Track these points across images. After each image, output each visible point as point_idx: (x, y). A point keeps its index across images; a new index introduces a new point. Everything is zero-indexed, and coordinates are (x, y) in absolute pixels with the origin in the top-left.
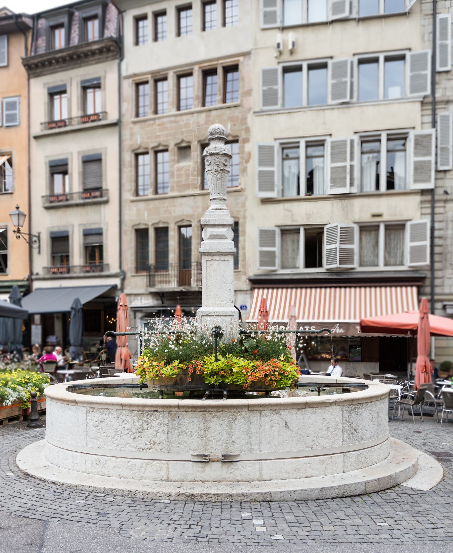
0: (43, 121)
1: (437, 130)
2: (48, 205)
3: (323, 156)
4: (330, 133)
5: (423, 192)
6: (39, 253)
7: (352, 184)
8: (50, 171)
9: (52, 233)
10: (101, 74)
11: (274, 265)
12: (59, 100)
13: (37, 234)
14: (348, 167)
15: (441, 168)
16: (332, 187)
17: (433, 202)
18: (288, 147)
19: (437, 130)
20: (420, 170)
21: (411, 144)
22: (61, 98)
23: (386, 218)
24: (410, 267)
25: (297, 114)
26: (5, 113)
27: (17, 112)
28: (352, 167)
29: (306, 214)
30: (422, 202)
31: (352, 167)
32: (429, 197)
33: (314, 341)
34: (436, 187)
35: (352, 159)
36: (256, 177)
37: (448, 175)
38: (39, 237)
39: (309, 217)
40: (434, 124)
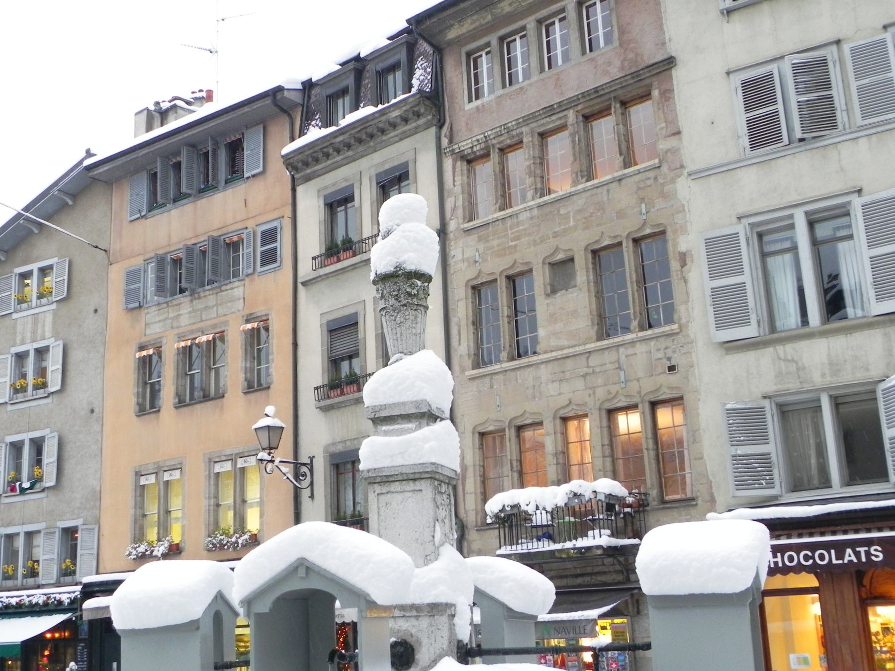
3: (850, 237)
4: (858, 185)
6: (312, 496)
8: (331, 348)
9: (333, 456)
10: (408, 157)
11: (771, 484)
12: (343, 213)
13: (308, 461)
16: (879, 298)
18: (768, 236)
27: (277, 244)
33: (70, 635)
36: (709, 301)
39: (839, 370)
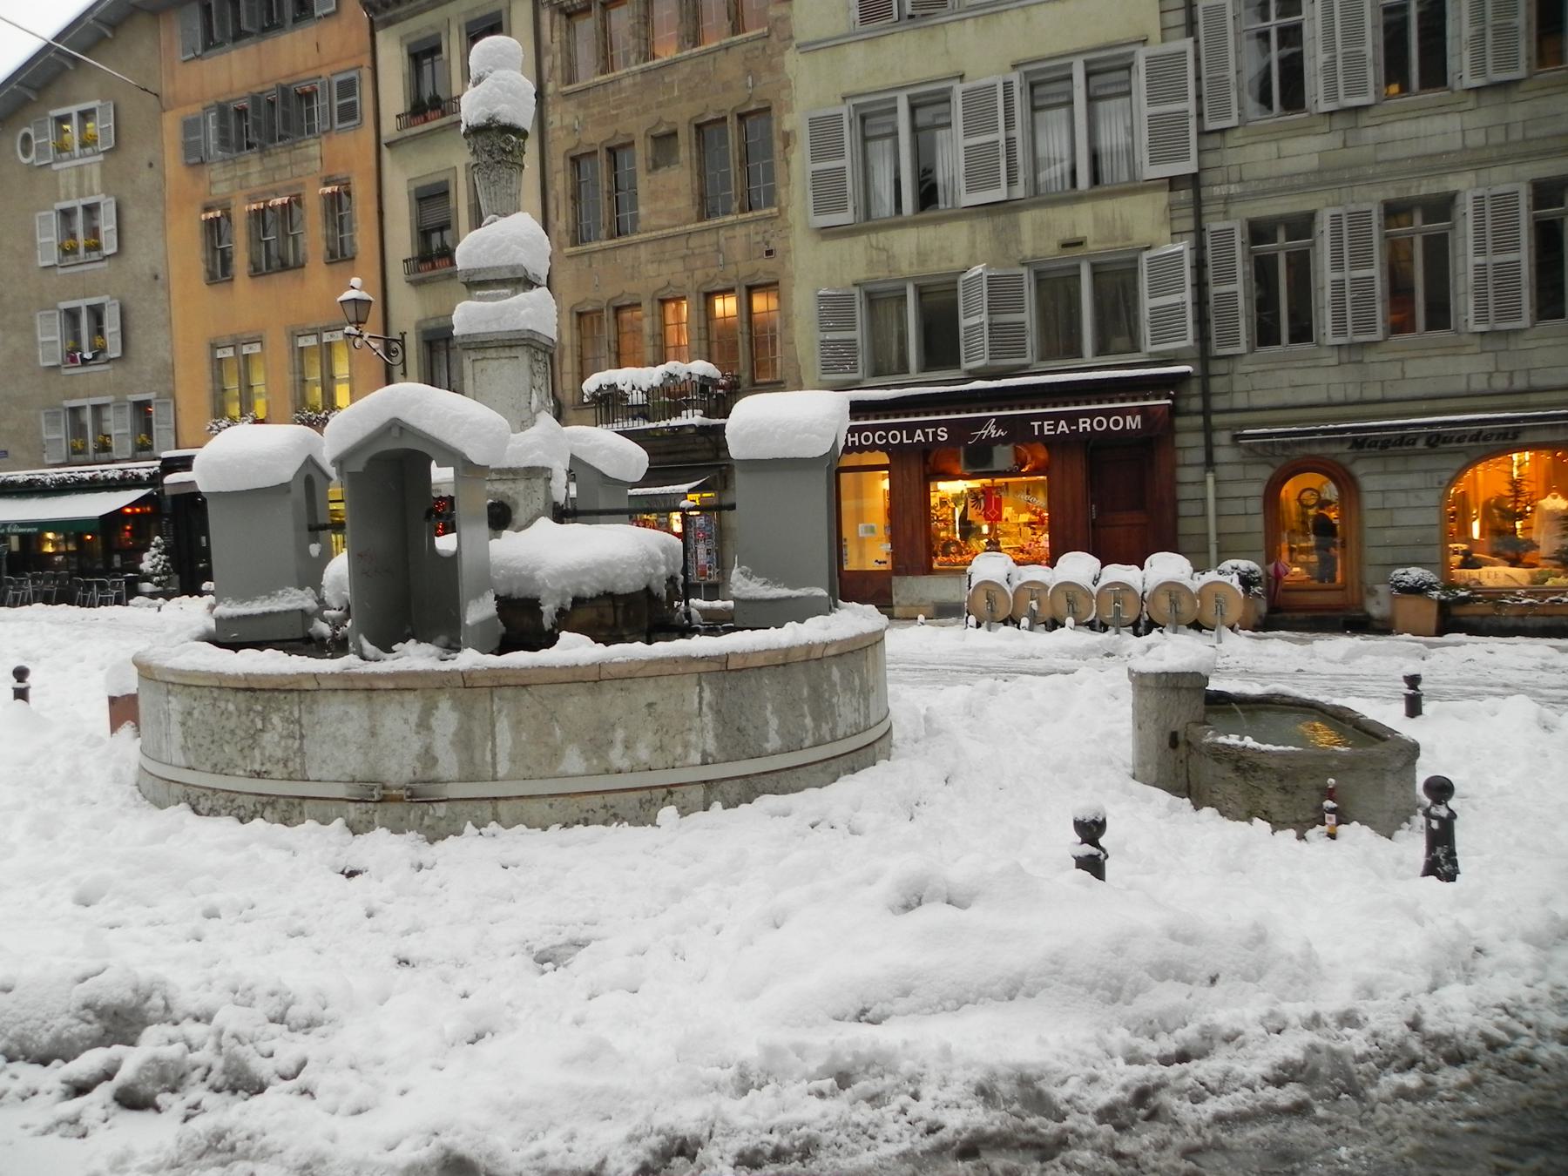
0: (401, 110)
1: (1197, 42)
2: (413, 277)
5: (1173, 183)
7: (1012, 181)
14: (1002, 142)
15: (1210, 125)
16: (969, 190)
17: (1198, 204)
18: (870, 119)
19: (1197, 42)
20: (1165, 137)
21: (1140, 80)
22: (433, 63)
23: (1091, 247)
24: (1151, 354)
25: (888, 39)
26: (336, 103)
27: (356, 98)
28: (1010, 142)
29: (919, 254)
30: (1171, 207)
31: (1010, 142)
32: (1184, 195)
34: (1201, 170)
35: (1009, 124)
37: (1231, 139)
38: (402, 342)
40: (1191, 27)
